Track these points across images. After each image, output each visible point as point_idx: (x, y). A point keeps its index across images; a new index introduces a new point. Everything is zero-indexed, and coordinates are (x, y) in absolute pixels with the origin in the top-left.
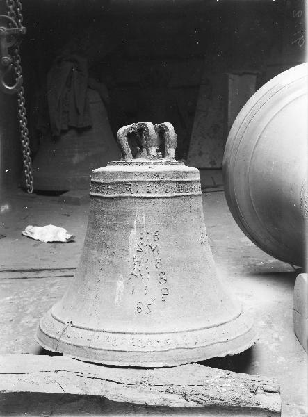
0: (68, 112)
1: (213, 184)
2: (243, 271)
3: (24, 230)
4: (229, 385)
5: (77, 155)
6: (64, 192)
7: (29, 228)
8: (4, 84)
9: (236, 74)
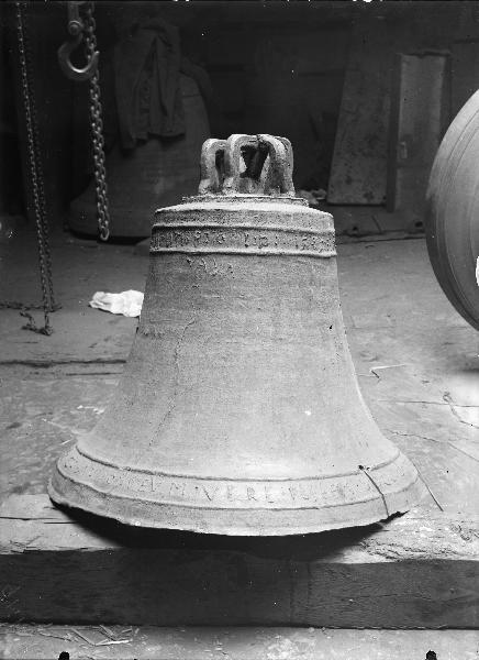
1: (376, 229)
4: (429, 530)
5: (162, 179)
6: (145, 238)
7: (98, 295)
8: (70, 65)
9: (412, 55)
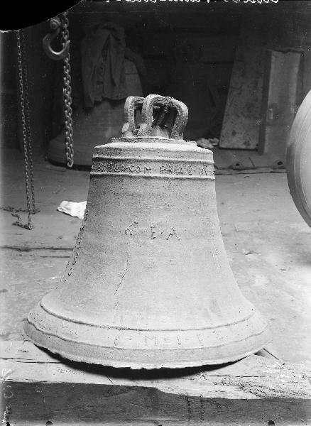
0: (102, 83)
2: (299, 259)
3: (59, 205)
7: (64, 203)
9: (280, 51)
